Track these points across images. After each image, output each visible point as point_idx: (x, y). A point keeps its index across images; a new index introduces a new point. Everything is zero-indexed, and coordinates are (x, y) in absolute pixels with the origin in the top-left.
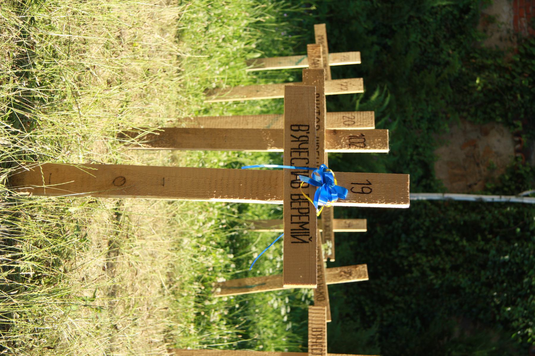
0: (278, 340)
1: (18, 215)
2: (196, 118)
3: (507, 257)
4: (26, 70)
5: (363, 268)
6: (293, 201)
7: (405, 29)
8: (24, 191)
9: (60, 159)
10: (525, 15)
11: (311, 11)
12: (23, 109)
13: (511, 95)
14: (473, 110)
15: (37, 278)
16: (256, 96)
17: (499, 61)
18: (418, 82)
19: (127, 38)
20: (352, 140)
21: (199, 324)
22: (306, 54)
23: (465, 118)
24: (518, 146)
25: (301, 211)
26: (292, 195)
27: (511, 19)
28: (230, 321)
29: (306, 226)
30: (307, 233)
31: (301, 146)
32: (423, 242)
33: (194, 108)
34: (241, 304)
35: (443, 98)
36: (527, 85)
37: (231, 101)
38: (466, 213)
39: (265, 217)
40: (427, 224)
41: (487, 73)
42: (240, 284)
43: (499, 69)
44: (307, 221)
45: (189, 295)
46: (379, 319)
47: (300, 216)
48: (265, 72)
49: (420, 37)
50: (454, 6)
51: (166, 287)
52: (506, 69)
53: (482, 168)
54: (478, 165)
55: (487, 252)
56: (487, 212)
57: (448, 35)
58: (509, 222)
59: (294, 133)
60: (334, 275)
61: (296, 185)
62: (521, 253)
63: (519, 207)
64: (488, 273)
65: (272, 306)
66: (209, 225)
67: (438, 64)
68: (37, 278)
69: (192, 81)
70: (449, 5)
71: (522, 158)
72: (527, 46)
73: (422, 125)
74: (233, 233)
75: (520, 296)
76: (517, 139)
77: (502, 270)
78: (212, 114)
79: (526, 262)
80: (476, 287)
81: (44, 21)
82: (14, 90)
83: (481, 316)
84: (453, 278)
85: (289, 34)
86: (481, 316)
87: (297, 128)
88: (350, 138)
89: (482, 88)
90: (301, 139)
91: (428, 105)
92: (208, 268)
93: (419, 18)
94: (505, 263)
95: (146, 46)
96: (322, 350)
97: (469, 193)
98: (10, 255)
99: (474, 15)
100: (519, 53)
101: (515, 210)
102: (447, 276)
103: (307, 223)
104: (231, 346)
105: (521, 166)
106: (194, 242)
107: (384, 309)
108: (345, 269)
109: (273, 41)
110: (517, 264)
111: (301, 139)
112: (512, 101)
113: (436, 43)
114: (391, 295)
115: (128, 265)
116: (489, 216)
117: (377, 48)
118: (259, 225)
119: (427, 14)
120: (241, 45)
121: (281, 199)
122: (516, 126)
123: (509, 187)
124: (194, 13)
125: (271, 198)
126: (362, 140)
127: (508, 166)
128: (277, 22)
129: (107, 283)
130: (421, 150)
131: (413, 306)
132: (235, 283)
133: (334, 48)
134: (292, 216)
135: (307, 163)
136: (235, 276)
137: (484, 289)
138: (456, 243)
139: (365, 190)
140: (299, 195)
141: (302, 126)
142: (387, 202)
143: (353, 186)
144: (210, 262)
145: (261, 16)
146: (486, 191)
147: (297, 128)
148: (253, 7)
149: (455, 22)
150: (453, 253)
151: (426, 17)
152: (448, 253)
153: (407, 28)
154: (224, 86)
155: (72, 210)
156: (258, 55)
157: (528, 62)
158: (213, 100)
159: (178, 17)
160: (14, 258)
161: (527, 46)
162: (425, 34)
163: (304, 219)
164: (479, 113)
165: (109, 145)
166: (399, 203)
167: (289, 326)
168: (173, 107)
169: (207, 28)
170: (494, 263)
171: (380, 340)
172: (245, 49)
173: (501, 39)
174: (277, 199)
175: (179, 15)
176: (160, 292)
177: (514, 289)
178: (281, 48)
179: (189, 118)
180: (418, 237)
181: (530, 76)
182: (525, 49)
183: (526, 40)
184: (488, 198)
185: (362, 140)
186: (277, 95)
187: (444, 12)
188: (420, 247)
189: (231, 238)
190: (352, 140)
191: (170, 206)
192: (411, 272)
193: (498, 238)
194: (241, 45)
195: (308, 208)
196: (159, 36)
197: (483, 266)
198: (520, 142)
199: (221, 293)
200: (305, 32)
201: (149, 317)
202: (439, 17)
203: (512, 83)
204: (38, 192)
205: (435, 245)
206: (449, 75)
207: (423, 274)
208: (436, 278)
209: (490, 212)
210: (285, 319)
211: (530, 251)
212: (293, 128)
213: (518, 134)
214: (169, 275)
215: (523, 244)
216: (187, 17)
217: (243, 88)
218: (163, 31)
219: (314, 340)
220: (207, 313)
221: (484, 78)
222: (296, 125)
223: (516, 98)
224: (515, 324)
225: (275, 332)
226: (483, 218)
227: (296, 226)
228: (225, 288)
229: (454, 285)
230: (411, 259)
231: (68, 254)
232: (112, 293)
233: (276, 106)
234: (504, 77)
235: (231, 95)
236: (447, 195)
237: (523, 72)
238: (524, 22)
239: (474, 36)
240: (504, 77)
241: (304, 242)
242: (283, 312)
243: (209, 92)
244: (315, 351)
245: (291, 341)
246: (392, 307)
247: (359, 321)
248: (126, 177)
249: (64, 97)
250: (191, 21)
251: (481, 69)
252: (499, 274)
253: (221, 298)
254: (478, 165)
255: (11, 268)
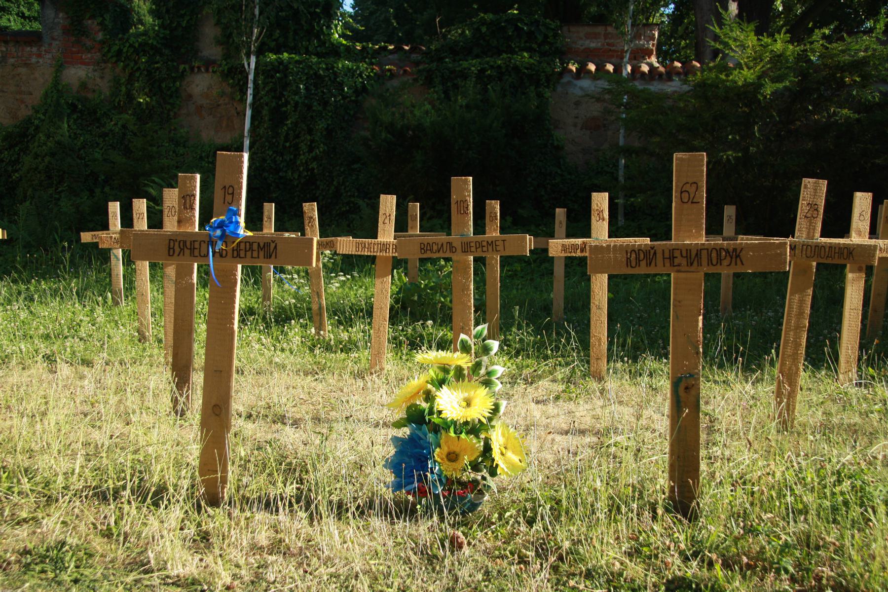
0: (367, 285)
1: (243, 497)
2: (166, 349)
3: (301, 86)
4: (111, 492)
5: (306, 206)
6: (238, 256)
7: (89, 163)
8: (223, 493)
9: (196, 463)
10: (80, 55)
11: (69, 247)
12: (148, 494)
13: (155, 72)
14: (168, 107)
15: (301, 481)
16: (147, 297)
17: (123, 80)
18: (140, 153)
19: (87, 408)
20: (188, 206)
21: (350, 349)
22: (109, 250)
23: (175, 113)
24: (203, 69)
25: (248, 249)
26: (233, 257)
27: (83, 67)
28: (349, 324)
29: (262, 245)
30: (268, 244)
31: (189, 247)
32: (287, 157)
33: (156, 351)
34: (335, 314)
35: (156, 132)
36: (146, 58)
37: (151, 320)
38: (262, 119)
39: (260, 293)
40: (271, 153)
41: (135, 92)
42: (317, 314)
43: (131, 80)
44: (257, 244)
45: (325, 358)
46: (352, 199)
47: (252, 250)
48: (126, 289)
49: (97, 150)
50: (69, 116)
51: (317, 376)
52: (131, 75)
53: (221, 102)
54: (219, 105)
55: (296, 104)
56: (262, 101)
57: (97, 125)
58: (271, 82)
59: (176, 254)
60: (311, 232)
61: (224, 253)
62: (298, 74)
63: (259, 74)
64: (315, 104)
65: (338, 288)
66: (264, 341)
67: (124, 134)
68: (301, 481)
69: (131, 353)
70: (68, 122)
71: (214, 67)
72: (110, 55)
73: (181, 152)
74: (273, 320)
75: (335, 79)
76: (196, 70)
77: (313, 92)
78: (162, 336)
79: (306, 71)
80: (326, 114)
81: (66, 479)
82: (129, 502)
83: (352, 112)
84: (319, 134)
85: (90, 268)
86: (352, 112)
87: (171, 251)
88: (185, 208)
89: (148, 97)
90: (182, 247)
91: (162, 146)
92: (302, 342)
93: (80, 150)
94: (307, 89)
95: (95, 392)
96: (374, 244)
97: (245, 115)
98: (279, 503)
99: (78, 100)
100: (116, 62)
101: (261, 77)
102: (317, 138)
103: (259, 243)
104: (370, 324)
105: (221, 69)
106: (279, 353)
107: (344, 195)
108: (306, 222)
109: (97, 282)
110: (307, 79)
111: (182, 247)
112: (160, 72)
113: (104, 135)
114: (333, 188)
115: (296, 408)
116: (266, 99)
117: (107, 189)
118: (266, 297)
119: (76, 142)
120: (99, 310)
121: (237, 267)
122: (184, 70)
123: (239, 80)
124: (66, 350)
125: (235, 275)
126: (188, 197)
127: (220, 79)
128: (78, 278)
129: (310, 424)
130: (203, 155)
131: (342, 169)
132: (316, 318)
133: (105, 226)
134: (252, 257)
135: (204, 242)
136: (310, 319)
137: (329, 108)
138: (289, 129)
139: (230, 191)
140: (233, 250)
141: (169, 245)
142: (241, 172)
143: (226, 202)
144: (297, 339)
145: (71, 291)
146: (243, 100)
147: (171, 251)
148: (62, 298)
149: (84, 117)
150: (297, 132)
151: (79, 144)
152: (297, 136)
153: (89, 161)
154: (136, 324)
155: (243, 454)
156: (109, 294)
157: (124, 55)
158: (150, 333)
159: (69, 364)
160: (282, 500)
161: (110, 55)
162: (96, 145)
163: (255, 246)
164: (171, 101)
165: (187, 424)
166: (243, 162)
167: (356, 274)
168: (154, 369)
169: (81, 339)
170: (306, 98)
171: (370, 199)
172: (103, 307)
173: (102, 78)
174: (237, 271)
175: (67, 363)
176: (321, 382)
177: (329, 83)
178: (103, 275)
179: (165, 354)
180: (282, 161)
181: (138, 54)
182: (112, 57)
183: (104, 55)
184: (250, 99)
185: (188, 197)
186: (146, 277)
187: (75, 127)
188: (291, 160)
189: (276, 321)
190: (188, 206)
191: (245, 373)
192: (313, 169)
193: (285, 93)
194: (99, 310)
195: (246, 242)
196: (87, 381)
197: (309, 107)
198: (199, 68)
199: (325, 331)
200: (90, 253)
201: (342, 391)
202: (79, 132)
203: (144, 70)
204: (224, 481)
205: (290, 147)
206: (135, 124)
207: (315, 159)
208: (318, 148)
209: (262, 98)
210: (349, 277)
211: (296, 67)
212: (171, 254)
213: (192, 69)
214: (306, 374)
215: (290, 73)
216: (70, 356)
217: (139, 308)
218: (82, 377)
219: (366, 250)
220: (341, 343)
221: (139, 94)
222: (169, 251)
223: (158, 68)
224: (359, 86)
225: (361, 287)
226: (267, 104)
227: (262, 254)
228: (320, 327)
229: (325, 133)
230: (301, 169)
231: (282, 457)
232: (317, 419)
233: (158, 281)
234: (138, 77)
235: (145, 319)
236: (246, 134)
237: (135, 60)
238: (86, 56)
239: (98, 101)
240: (138, 77)
241: (276, 247)
242: (343, 278)
243: (142, 338)
244: (376, 250)
245: (369, 274)
246: (343, 187)
247: (354, 216)
248: (213, 404)
249: (139, 461)
250: (74, 353)
251: (130, 97)
252: (316, 94)
253: (329, 331)
254: (219, 105)
255: (290, 502)
